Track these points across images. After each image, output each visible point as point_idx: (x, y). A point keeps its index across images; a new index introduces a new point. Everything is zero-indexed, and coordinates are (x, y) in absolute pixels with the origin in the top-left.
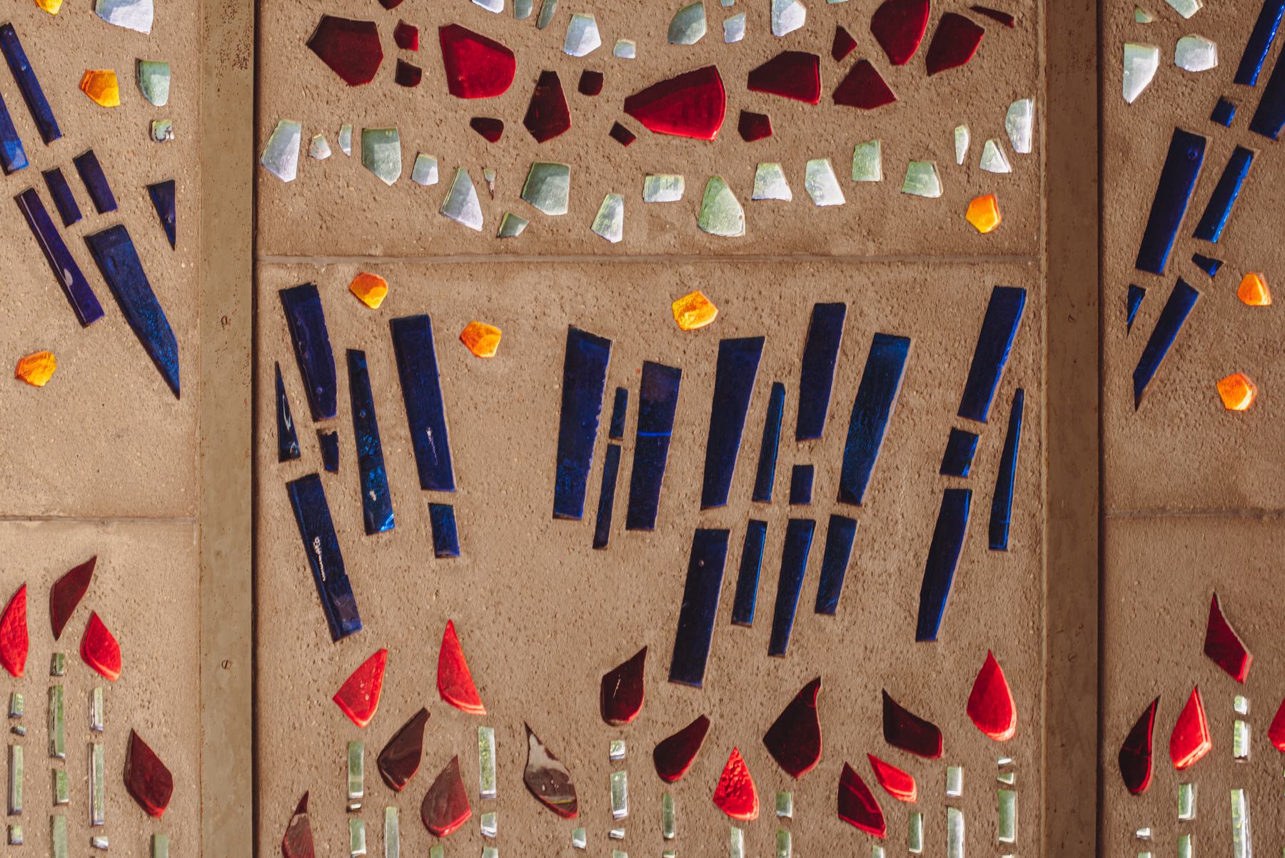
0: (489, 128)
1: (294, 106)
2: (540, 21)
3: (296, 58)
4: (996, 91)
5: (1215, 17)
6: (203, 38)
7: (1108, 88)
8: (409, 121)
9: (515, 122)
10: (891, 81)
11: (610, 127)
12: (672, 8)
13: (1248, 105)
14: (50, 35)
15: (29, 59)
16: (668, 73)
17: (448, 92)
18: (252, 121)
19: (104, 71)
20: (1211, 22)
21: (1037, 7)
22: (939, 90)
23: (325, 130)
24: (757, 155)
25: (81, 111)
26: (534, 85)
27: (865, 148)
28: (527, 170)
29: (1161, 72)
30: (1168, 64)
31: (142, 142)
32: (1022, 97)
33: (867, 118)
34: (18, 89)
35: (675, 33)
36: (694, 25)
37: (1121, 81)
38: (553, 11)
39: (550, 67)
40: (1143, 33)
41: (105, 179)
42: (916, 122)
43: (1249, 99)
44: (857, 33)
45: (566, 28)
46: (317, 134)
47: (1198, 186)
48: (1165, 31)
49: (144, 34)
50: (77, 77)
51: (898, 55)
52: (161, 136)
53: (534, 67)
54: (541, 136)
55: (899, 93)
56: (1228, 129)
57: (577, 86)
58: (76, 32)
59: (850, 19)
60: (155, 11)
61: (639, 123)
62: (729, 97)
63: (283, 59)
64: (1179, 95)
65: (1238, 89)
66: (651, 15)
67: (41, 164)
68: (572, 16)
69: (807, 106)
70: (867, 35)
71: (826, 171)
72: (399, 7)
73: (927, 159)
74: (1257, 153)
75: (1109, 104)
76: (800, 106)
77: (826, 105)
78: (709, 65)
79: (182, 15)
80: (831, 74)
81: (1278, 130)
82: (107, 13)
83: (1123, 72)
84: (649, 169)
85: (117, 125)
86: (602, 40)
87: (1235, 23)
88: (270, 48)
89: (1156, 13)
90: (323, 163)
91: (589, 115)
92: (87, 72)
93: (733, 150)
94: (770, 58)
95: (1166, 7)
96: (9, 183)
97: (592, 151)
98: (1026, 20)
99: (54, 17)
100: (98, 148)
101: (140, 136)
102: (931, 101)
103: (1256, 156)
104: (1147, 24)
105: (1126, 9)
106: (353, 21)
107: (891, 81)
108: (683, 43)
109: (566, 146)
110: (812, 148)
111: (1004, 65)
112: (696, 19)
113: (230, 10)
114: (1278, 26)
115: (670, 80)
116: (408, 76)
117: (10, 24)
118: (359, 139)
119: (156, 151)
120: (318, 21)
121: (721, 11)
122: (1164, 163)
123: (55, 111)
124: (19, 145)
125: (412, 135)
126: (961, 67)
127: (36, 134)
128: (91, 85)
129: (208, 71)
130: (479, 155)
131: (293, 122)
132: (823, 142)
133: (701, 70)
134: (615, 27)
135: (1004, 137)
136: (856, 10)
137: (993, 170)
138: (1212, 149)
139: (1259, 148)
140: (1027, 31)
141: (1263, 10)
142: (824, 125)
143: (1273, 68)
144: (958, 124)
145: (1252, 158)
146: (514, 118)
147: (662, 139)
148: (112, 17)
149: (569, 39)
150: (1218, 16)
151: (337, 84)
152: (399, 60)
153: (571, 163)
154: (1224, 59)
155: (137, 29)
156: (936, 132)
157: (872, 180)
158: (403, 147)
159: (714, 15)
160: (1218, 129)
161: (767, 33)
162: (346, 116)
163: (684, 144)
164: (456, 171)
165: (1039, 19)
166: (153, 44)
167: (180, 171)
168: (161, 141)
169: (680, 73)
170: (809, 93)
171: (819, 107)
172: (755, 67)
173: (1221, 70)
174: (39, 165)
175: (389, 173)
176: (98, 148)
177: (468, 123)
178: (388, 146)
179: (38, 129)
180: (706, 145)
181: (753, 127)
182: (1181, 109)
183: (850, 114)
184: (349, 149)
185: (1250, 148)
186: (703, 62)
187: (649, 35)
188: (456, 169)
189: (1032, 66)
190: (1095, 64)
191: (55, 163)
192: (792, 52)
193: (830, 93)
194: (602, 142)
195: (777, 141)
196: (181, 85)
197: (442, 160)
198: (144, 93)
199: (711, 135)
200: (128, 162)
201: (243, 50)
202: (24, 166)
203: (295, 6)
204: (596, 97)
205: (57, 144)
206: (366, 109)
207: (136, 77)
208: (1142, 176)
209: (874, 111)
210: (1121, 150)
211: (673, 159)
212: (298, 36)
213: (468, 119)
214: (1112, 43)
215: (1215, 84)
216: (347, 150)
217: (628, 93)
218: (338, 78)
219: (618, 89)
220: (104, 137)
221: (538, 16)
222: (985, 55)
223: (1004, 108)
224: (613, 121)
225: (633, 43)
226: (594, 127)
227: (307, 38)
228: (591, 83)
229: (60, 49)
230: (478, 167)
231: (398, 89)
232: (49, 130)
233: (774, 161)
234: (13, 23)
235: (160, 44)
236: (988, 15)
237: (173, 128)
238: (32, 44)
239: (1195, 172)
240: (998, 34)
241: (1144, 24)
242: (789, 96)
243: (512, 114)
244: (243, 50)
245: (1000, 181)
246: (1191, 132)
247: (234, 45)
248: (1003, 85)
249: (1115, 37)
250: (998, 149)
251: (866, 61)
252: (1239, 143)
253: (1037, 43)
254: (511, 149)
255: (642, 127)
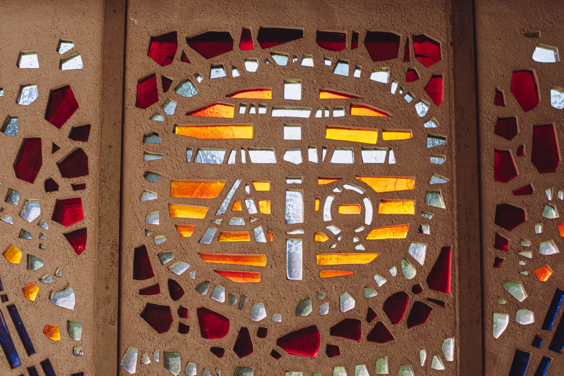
0: (218, 352)
1: (135, 342)
2: (241, 306)
3: (136, 321)
4: (438, 334)
5: (533, 301)
6: (96, 313)
7: (487, 333)
8: (184, 348)
9: (229, 349)
10: (392, 331)
11: (270, 351)
12: (297, 300)
13: (548, 338)
14: (31, 310)
15: (22, 319)
16: (295, 328)
17: (201, 336)
18: (117, 348)
19: (54, 325)
20: (531, 303)
21: (455, 298)
22: (413, 335)
23: (148, 352)
24: (334, 363)
25: (44, 342)
26: (238, 333)
27: (381, 359)
28: (234, 370)
29: (510, 325)
30: (513, 322)
31: (70, 356)
32: (449, 337)
33: (382, 347)
34: (17, 333)
35: (299, 311)
36: (307, 307)
37: (492, 330)
38: (246, 302)
39: (244, 325)
40: (502, 309)
41: (54, 371)
42: (403, 348)
43: (549, 336)
44: (377, 311)
45: (251, 309)
46: (145, 354)
47: (526, 374)
48: (511, 308)
49: (71, 310)
50: (42, 328)
51: (395, 320)
52: (78, 354)
53: (238, 325)
54: (241, 355)
55: (395, 336)
56: (539, 349)
57: (256, 334)
58: (42, 309)
59: (374, 304)
60: (76, 300)
61: (283, 350)
62: (322, 338)
63: (130, 321)
64: (518, 335)
65: (543, 332)
66: (288, 304)
67: (27, 364)
68: (254, 304)
69: (356, 342)
70: (382, 311)
71: (364, 370)
72: (180, 300)
73: (408, 364)
74: (552, 359)
75: (487, 340)
76: (352, 342)
77: (364, 341)
78: (313, 325)
79: (87, 302)
80: (366, 328)
81: (561, 349)
82: (55, 300)
83: (493, 325)
84: (287, 369)
85: (59, 348)
86: (267, 314)
87: (542, 303)
88: (125, 317)
89: (507, 300)
90: (147, 366)
91: (262, 346)
92: (46, 325)
93: (324, 361)
94: (339, 321)
95: (511, 297)
96: (13, 372)
97: (263, 362)
98: (451, 304)
99: (33, 302)
100: (51, 358)
101: (69, 353)
102: (410, 339)
103: (552, 360)
104: (503, 305)
105: (494, 299)
106: (160, 305)
107: (392, 331)
108: (302, 315)
109: (251, 360)
110: (358, 360)
111: (441, 324)
112: (308, 305)
113: (107, 301)
114: (561, 304)
115: (296, 331)
116: (184, 329)
117: (14, 304)
118: (162, 356)
119: (76, 360)
120: (145, 305)
121: (318, 302)
122: (511, 364)
123: (33, 342)
124: (17, 356)
125: (185, 354)
126: (422, 324)
127: (25, 352)
128: (48, 331)
129: (98, 326)
130: (214, 363)
131: (134, 349)
132: (363, 357)
133: (310, 327)
134: (272, 309)
135: (442, 355)
136: (377, 301)
137: (436, 368)
138: (532, 358)
139: (553, 357)
140: (451, 309)
141: (554, 297)
142: (363, 350)
143: (558, 323)
144: (421, 349)
145: (550, 361)
146: (229, 348)
147: (293, 357)
148: (57, 302)
149: (253, 313)
150: (534, 301)
151: (153, 333)
152: (180, 322)
153: (254, 367)
154: (537, 319)
155: (68, 308)
156: (412, 352)
157: (384, 373)
158: (181, 359)
159: (315, 303)
160: (535, 349)
161: (338, 311)
162: (157, 346)
163: (303, 359)
164: (204, 370)
165: (456, 303)
166: (75, 314)
167: (86, 368)
168: (78, 355)
169: (300, 328)
170: (356, 336)
171: (361, 343)
172: (333, 326)
173: (536, 324)
174: (26, 365)
175: (175, 370)
176: (51, 358)
177: (209, 349)
178: (175, 359)
179: (26, 350)
180: (312, 359)
181: (332, 351)
182: (519, 341)
183: (374, 346)
184: (158, 360)
185: (549, 357)
186: (311, 324)
187: (287, 312)
188: (204, 369)
189: (453, 324)
190: (481, 323)
191: (33, 364)
192: (349, 319)
193: (366, 337)
194: (267, 358)
195: (343, 357)
196: (87, 332)
197: (198, 366)
198: (71, 335)
199: (314, 355)
200: (64, 364)
201: (113, 318)
202: (19, 365)
203: (135, 299)
204: (265, 339)
205: (34, 356)
206: (166, 343)
207: (67, 328)
208: (502, 370)
209: (385, 344)
210: (492, 359)
211: (298, 365)
212: (137, 312)
213: (209, 348)
214: (488, 313)
215: (533, 330)
216: (158, 360)
217: (278, 337)
218: (154, 330)
219: (274, 335)
220: (54, 353)
221: (239, 304)
222: (433, 319)
223: (441, 342)
224: (272, 349)
225: (281, 315)
226: (264, 351)
227: (140, 313)
228: (262, 332)
229: (35, 316)
230: (214, 368)
231: (179, 335)
232: (30, 350)
233: (342, 366)
234: (15, 304)
235: (78, 314)
236: (434, 302)
237: (83, 350)
238: (23, 313)
239: (526, 368)
240: (438, 310)
241: (502, 305)
242: (348, 338)
243: (228, 346)
244: (113, 318)
245: (440, 373)
246: (523, 351)
247: (109, 316)
248: (440, 332)
249: (489, 310)
250: (439, 359)
251: (381, 322)
252: (544, 355)
253: (455, 314)
254: (228, 361)
255: (285, 352)
